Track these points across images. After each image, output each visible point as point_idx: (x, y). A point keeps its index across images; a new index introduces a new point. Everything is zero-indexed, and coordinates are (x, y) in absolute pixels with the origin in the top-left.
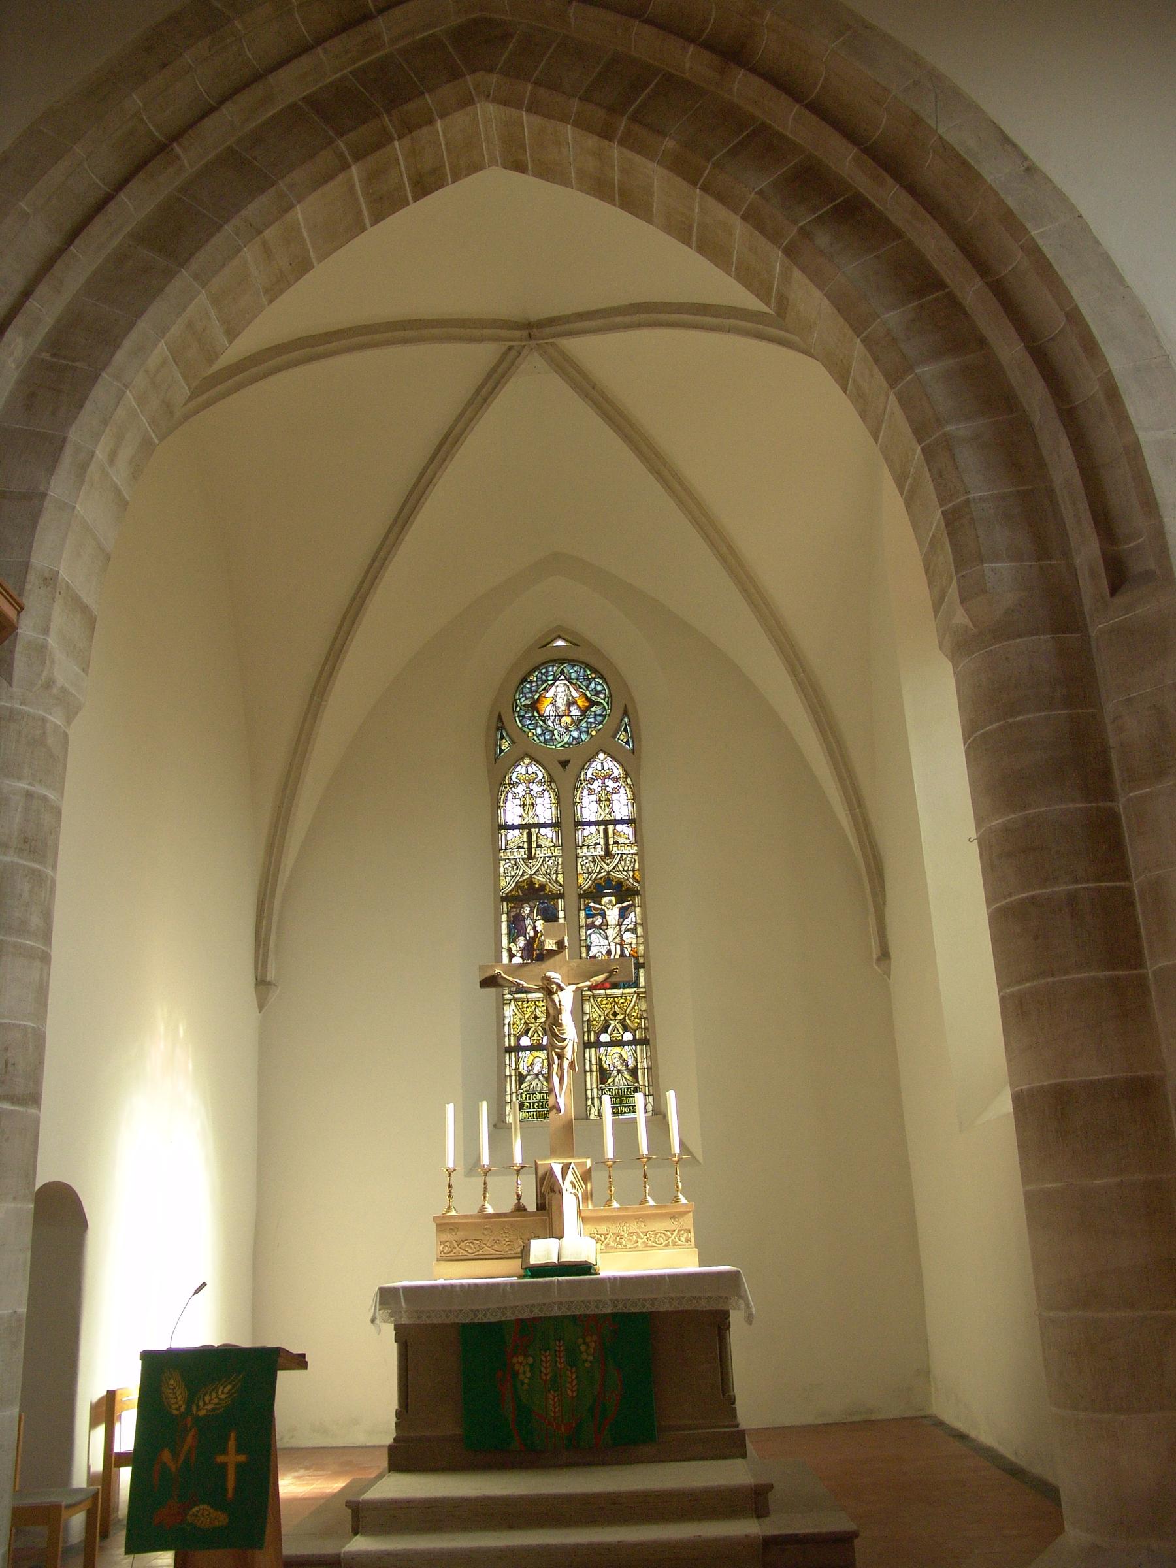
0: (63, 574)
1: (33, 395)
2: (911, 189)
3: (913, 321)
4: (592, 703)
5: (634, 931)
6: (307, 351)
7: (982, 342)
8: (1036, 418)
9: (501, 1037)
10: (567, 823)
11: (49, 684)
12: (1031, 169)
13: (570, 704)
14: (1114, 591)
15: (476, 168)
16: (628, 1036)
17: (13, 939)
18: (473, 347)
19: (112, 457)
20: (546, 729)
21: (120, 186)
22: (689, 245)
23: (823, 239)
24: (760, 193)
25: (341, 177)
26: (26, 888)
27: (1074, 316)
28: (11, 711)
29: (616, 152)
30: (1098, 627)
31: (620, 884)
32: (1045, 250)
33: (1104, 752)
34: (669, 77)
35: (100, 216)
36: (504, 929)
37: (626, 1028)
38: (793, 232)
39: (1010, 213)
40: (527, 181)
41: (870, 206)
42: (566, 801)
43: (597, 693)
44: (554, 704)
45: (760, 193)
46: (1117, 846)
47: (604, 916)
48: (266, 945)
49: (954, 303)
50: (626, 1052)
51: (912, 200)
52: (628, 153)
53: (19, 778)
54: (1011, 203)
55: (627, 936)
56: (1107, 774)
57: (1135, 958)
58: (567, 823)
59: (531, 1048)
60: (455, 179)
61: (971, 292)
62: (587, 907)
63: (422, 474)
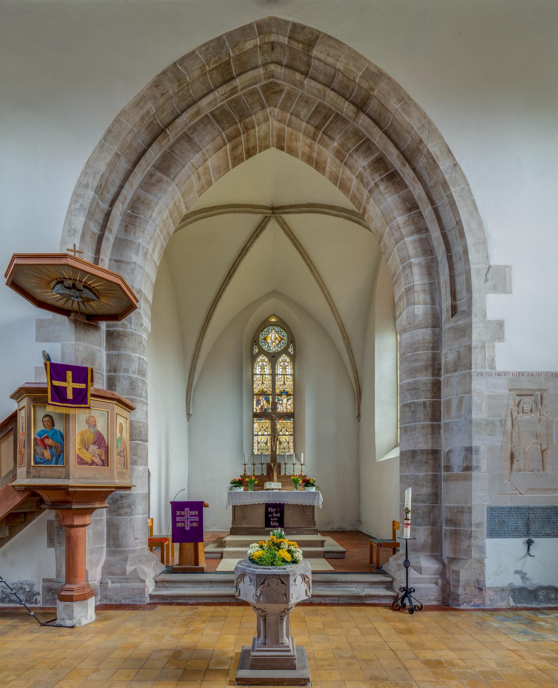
0: (143, 290)
1: (127, 226)
2: (414, 170)
3: (406, 221)
4: (282, 339)
5: (290, 405)
6: (204, 214)
7: (427, 230)
8: (439, 259)
9: (253, 432)
10: (273, 375)
11: (142, 325)
12: (456, 165)
13: (276, 339)
14: (452, 316)
16: (287, 433)
17: (138, 398)
18: (255, 215)
19: (154, 250)
20: (268, 346)
21: (149, 146)
22: (336, 186)
23: (382, 187)
24: (364, 167)
25: (224, 148)
26: (141, 384)
27: (459, 223)
28: (132, 333)
29: (316, 146)
30: (446, 326)
31: (287, 392)
32: (455, 197)
33: (440, 364)
34: (337, 115)
35: (143, 157)
37: (287, 431)
38: (372, 184)
39: (445, 182)
40: (284, 154)
41: (399, 175)
42: (273, 368)
43: (284, 336)
44: (271, 339)
45: (364, 167)
46: (439, 390)
47: (282, 400)
48: (189, 404)
49: (420, 215)
50: (286, 437)
51: (414, 175)
52: (320, 146)
53: (136, 353)
54: (447, 177)
55: (288, 406)
56: (440, 369)
57: (439, 419)
58: (273, 375)
59: (262, 435)
60: (260, 152)
61: (427, 211)
62: (278, 398)
63: (236, 261)
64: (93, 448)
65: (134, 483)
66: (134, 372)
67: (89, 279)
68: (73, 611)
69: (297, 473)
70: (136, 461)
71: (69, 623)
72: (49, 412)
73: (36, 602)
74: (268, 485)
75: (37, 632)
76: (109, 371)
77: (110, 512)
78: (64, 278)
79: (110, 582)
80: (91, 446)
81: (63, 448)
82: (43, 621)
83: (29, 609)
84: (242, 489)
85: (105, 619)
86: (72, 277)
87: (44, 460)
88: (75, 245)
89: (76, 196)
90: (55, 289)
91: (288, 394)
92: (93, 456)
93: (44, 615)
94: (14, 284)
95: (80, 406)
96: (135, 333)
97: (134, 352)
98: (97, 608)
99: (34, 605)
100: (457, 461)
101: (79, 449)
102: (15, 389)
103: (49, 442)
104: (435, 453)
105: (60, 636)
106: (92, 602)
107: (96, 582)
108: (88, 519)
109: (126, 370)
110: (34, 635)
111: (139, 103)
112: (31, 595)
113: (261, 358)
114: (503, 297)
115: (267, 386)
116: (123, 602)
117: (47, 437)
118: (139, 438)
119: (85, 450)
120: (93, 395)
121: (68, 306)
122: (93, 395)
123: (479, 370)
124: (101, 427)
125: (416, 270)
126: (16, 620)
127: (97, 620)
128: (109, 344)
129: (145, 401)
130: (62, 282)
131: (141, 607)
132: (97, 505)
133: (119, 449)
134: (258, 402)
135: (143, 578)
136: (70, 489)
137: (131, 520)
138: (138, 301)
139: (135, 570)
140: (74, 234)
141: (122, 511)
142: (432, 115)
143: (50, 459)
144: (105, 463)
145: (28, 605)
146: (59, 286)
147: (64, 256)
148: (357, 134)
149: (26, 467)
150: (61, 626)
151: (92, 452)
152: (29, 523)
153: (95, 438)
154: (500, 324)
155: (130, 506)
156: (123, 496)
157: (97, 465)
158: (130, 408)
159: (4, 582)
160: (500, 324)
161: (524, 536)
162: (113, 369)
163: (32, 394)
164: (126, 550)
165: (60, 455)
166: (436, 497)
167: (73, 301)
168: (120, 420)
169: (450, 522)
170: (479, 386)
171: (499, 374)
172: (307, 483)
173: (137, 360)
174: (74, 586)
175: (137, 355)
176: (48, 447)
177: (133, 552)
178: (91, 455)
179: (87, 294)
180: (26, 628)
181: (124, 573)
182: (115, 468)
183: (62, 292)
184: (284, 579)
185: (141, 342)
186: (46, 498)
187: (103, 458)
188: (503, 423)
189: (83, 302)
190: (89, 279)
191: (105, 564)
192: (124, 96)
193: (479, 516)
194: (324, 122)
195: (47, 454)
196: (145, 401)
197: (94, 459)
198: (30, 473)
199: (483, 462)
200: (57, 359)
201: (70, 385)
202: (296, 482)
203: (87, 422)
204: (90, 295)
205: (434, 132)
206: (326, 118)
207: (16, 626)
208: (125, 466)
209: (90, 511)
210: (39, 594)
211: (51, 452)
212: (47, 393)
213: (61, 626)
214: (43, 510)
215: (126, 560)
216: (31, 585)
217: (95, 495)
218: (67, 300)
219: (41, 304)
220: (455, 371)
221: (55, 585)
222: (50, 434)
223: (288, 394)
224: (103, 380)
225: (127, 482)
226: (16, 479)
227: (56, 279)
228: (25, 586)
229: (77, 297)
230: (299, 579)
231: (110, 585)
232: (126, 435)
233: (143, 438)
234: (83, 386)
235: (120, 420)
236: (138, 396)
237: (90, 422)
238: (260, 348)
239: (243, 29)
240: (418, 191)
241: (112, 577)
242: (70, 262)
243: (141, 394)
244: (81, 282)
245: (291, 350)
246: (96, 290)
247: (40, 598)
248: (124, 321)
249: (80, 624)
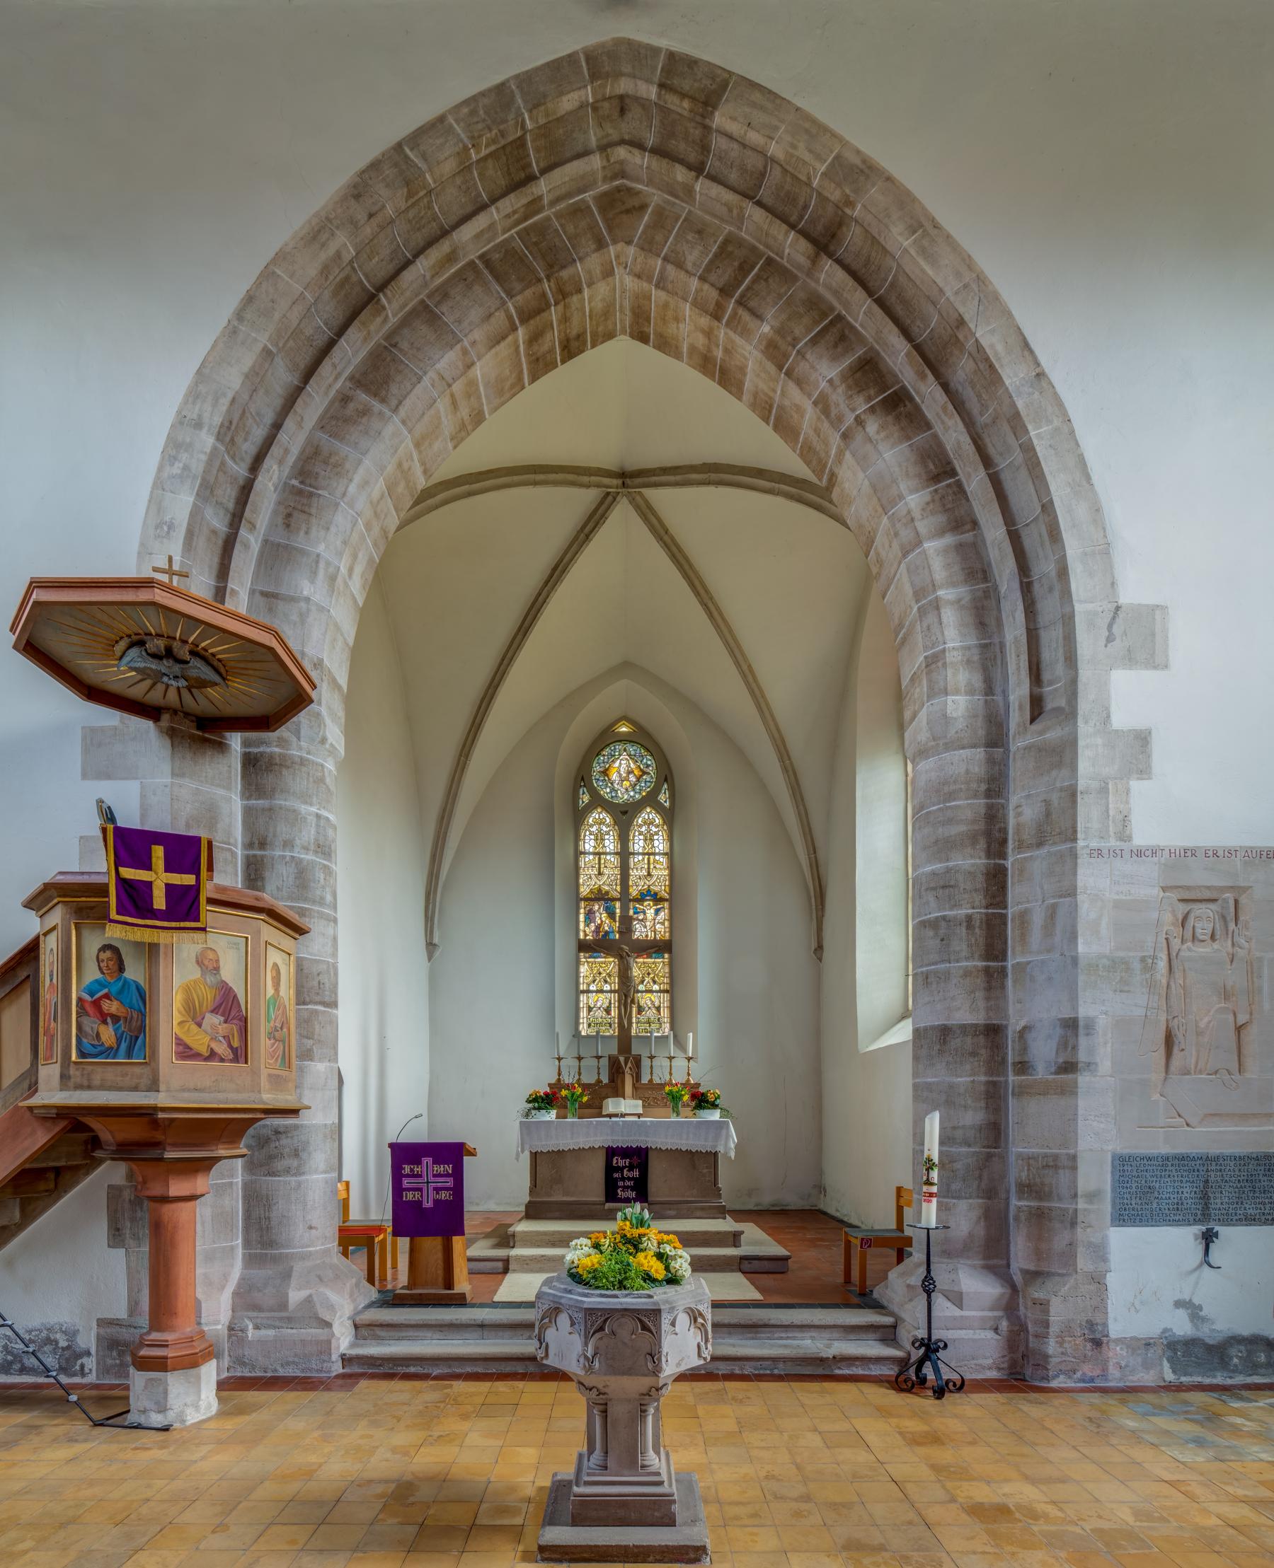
0: (326, 662)
1: (289, 515)
2: (945, 387)
3: (928, 504)
4: (644, 773)
5: (663, 924)
6: (466, 488)
7: (975, 524)
8: (1003, 589)
9: (577, 984)
10: (624, 854)
11: (324, 741)
12: (1040, 375)
13: (630, 772)
14: (1032, 721)
15: (610, 336)
16: (656, 987)
17: (316, 908)
18: (583, 491)
19: (351, 570)
20: (613, 790)
21: (341, 332)
22: (768, 423)
23: (872, 427)
26: (322, 876)
27: (1048, 508)
28: (301, 758)
29: (722, 333)
30: (1017, 743)
31: (656, 894)
32: (1038, 449)
34: (770, 261)
35: (327, 359)
36: (582, 917)
37: (655, 982)
38: (850, 419)
39: (1017, 415)
40: (648, 352)
41: (911, 399)
42: (624, 839)
43: (648, 766)
44: (619, 772)
45: (830, 381)
46: (1003, 888)
47: (644, 913)
48: (432, 920)
49: (960, 489)
50: (654, 997)
51: (945, 398)
52: (731, 334)
53: (311, 805)
54: (1020, 404)
55: (658, 926)
56: (1004, 842)
57: (1002, 956)
58: (624, 854)
59: (597, 992)
60: (593, 347)
61: (975, 481)
63: (539, 594)
64: (213, 1020)
65: (306, 1102)
66: (306, 849)
67: (202, 637)
68: (166, 1392)
69: (679, 1078)
70: (310, 1050)
71: (156, 1419)
72: (112, 938)
73: (82, 1372)
74: (611, 1105)
75: (86, 1441)
76: (249, 845)
78: (146, 634)
79: (251, 1327)
80: (208, 1015)
81: (143, 1021)
82: (98, 1415)
83: (67, 1389)
84: (552, 1115)
85: (240, 1411)
87: (99, 1049)
88: (170, 559)
89: (174, 447)
90: (126, 659)
91: (657, 899)
92: (213, 1039)
93: (102, 1401)
94: (32, 648)
95: (182, 924)
96: (308, 760)
97: (306, 803)
98: (222, 1386)
99: (77, 1380)
100: (1043, 1051)
101: (180, 1024)
102: (34, 886)
103: (112, 1007)
104: (993, 1032)
105: (136, 1449)
106: (210, 1373)
107: (219, 1327)
108: (201, 1183)
109: (288, 844)
110: (79, 1448)
111: (316, 234)
112: (71, 1357)
113: (596, 815)
114: (1149, 676)
115: (609, 880)
116: (281, 1372)
117: (107, 996)
118: (318, 998)
119: (194, 1027)
120: (211, 901)
121: (155, 697)
122: (211, 901)
123: (1094, 844)
124: (231, 972)
125: (949, 616)
126: (36, 1413)
127: (221, 1414)
128: (250, 784)
129: (332, 913)
130: (141, 643)
131: (322, 1383)
132: (222, 1152)
133: (272, 1024)
134: (590, 915)
135: (327, 1318)
136: (161, 1115)
137: (299, 1184)
138: (314, 687)
139: (309, 1300)
140: (168, 533)
141: (280, 1165)
142: (987, 263)
143: (115, 1046)
144: (240, 1054)
145: (64, 1379)
146: (134, 652)
147: (147, 584)
148: (815, 305)
149: (58, 1065)
150: (139, 1427)
151: (209, 1030)
152: (66, 1192)
153: (218, 998)
154: (1142, 739)
155: (296, 1154)
156: (281, 1130)
157: (222, 1060)
158: (298, 930)
159: (10, 1326)
160: (1142, 739)
161: (1196, 1222)
162: (258, 841)
163: (73, 898)
164: (287, 1254)
165: (137, 1038)
166: (995, 1132)
167: (168, 686)
168: (274, 957)
169: (1027, 1189)
170: (1093, 879)
171: (1140, 853)
172: (701, 1101)
173: (312, 820)
174: (169, 1336)
175: (314, 809)
176: (109, 1020)
177: (304, 1257)
178: (208, 1038)
179: (199, 669)
180: (60, 1430)
181: (283, 1306)
182: (262, 1066)
183: (142, 665)
184: (648, 1321)
185: (321, 780)
186: (105, 1136)
187: (236, 1044)
188: (1148, 965)
189: (189, 689)
190: (202, 637)
191: (239, 1285)
192: (282, 218)
193: (1094, 1176)
194: (741, 277)
195: (108, 1034)
196: (332, 913)
197: (213, 1045)
198: (69, 1077)
199: (1103, 1053)
200: (129, 818)
201: (159, 878)
202: (675, 1098)
203: (198, 962)
204: (206, 673)
205: (991, 300)
206: (744, 269)
207: (36, 1427)
208: (286, 1061)
209: (206, 1165)
210: (88, 1353)
211: (116, 1030)
212: (108, 896)
213: (139, 1427)
214: (98, 1162)
215: (287, 1276)
216: (72, 1334)
217: (218, 1129)
218: (154, 684)
219: (94, 693)
220: (1040, 844)
221: (125, 1334)
222: (114, 990)
223: (657, 899)
224: (236, 866)
225: (289, 1097)
226: (36, 1091)
227: (129, 636)
228: (58, 1336)
229: (176, 677)
230: (683, 1320)
231: (251, 1333)
232: (287, 992)
233: (327, 999)
234: (189, 879)
235: (274, 957)
236: (314, 902)
237: (206, 962)
238: (594, 793)
239: (555, 66)
240: (953, 436)
241: (255, 1314)
242: (160, 596)
243: (322, 898)
244: (185, 642)
245: (663, 798)
246: (219, 660)
247: (90, 1363)
248: (283, 732)
249: (183, 1421)
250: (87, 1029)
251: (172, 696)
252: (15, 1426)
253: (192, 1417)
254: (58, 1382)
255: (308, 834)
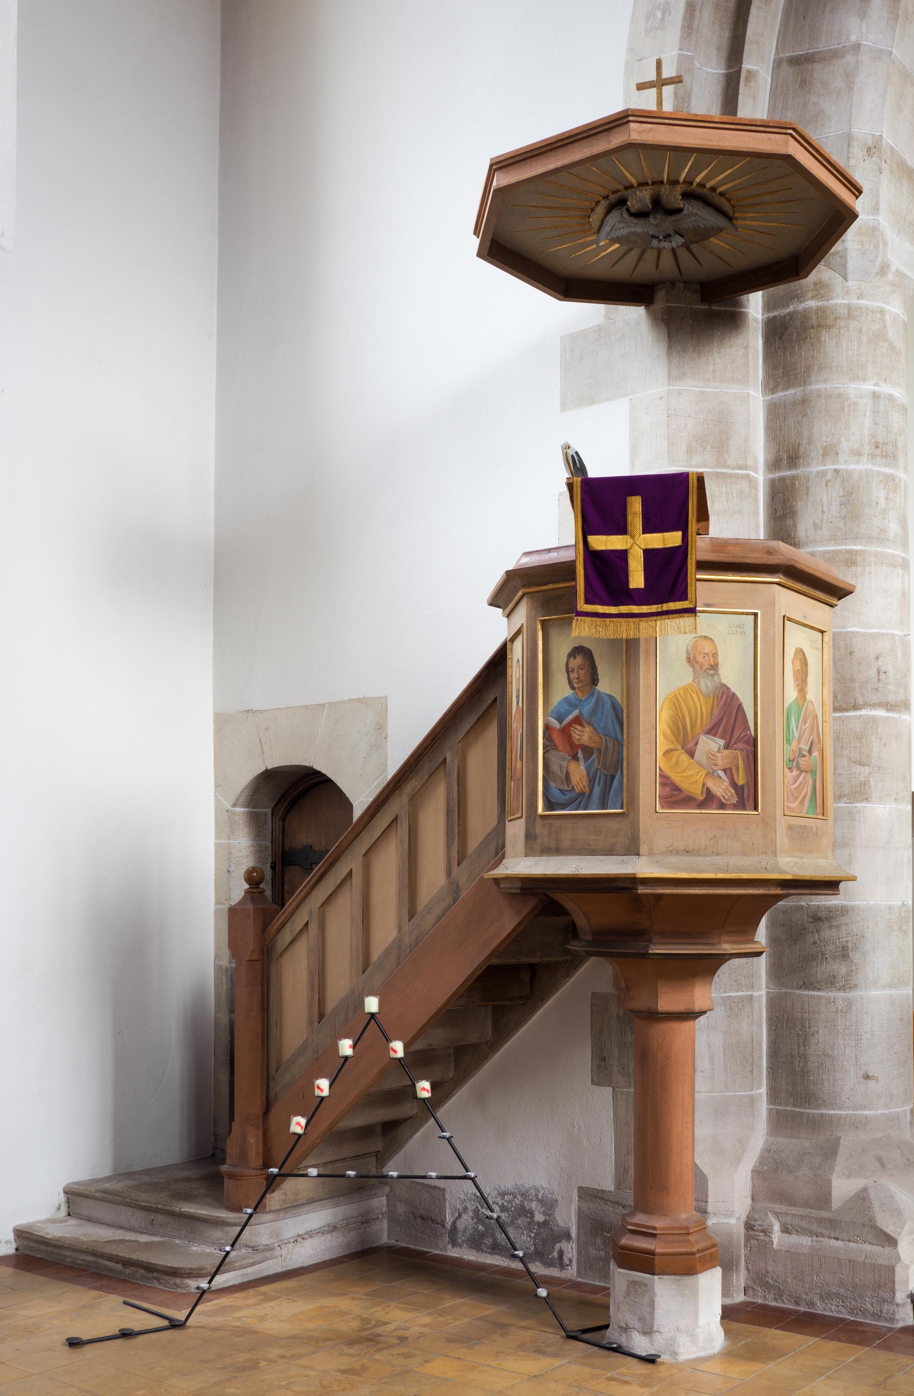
0: (888, 139)
11: (884, 269)
26: (882, 494)
28: (849, 308)
64: (710, 745)
65: (856, 873)
66: (857, 454)
67: (695, 170)
68: (652, 1305)
70: (865, 784)
71: (640, 1344)
72: (580, 638)
73: (561, 1263)
75: (555, 1355)
76: (774, 464)
77: (781, 972)
78: (626, 188)
79: (777, 1227)
80: (703, 739)
81: (620, 753)
82: (574, 1324)
83: (538, 1282)
85: (755, 1354)
86: (649, 177)
87: (570, 795)
88: (659, 63)
90: (606, 229)
92: (710, 774)
93: (584, 1305)
94: (502, 248)
95: (666, 607)
96: (859, 308)
97: (856, 378)
98: (729, 1314)
99: (554, 1272)
101: (667, 753)
102: (495, 579)
103: (583, 735)
105: (611, 1379)
106: (710, 1283)
107: (733, 1221)
108: (701, 995)
109: (830, 452)
110: (545, 1363)
112: (549, 1237)
116: (819, 1309)
117: (577, 720)
118: (876, 698)
119: (685, 757)
120: (704, 566)
121: (646, 271)
122: (704, 566)
124: (734, 674)
126: (503, 1308)
127: (728, 1355)
128: (775, 368)
129: (899, 553)
130: (621, 202)
131: (879, 1336)
132: (727, 947)
133: (794, 746)
135: (890, 1230)
136: (642, 890)
137: (849, 1003)
138: (857, 191)
139: (862, 1197)
140: (663, 18)
141: (821, 971)
143: (587, 790)
144: (747, 796)
145: (537, 1268)
146: (614, 217)
147: (620, 121)
149: (523, 821)
150: (619, 1350)
151: (705, 761)
152: (543, 1000)
153: (716, 711)
155: (844, 954)
156: (822, 914)
157: (722, 806)
158: (833, 592)
159: (473, 1179)
162: (787, 454)
163: (533, 587)
164: (831, 1117)
165: (613, 778)
167: (659, 251)
168: (797, 638)
173: (866, 404)
174: (659, 1223)
175: (869, 387)
176: (580, 755)
177: (858, 1124)
178: (703, 773)
179: (697, 215)
180: (527, 1335)
181: (823, 1199)
182: (779, 813)
183: (624, 232)
185: (881, 335)
186: (581, 921)
187: (741, 780)
189: (687, 246)
190: (695, 170)
191: (762, 1160)
195: (579, 773)
196: (899, 553)
197: (711, 784)
198: (535, 836)
200: (598, 468)
201: (636, 543)
203: (689, 660)
204: (708, 218)
207: (503, 1326)
208: (818, 803)
209: (708, 966)
210: (568, 1237)
211: (588, 768)
212: (574, 579)
213: (619, 1350)
214: (575, 962)
215: (830, 1152)
216: (549, 1205)
217: (717, 914)
218: (643, 253)
219: (568, 286)
221: (613, 1215)
222: (586, 709)
224: (756, 500)
225: (822, 862)
226: (503, 857)
227: (606, 197)
228: (534, 1205)
229: (667, 237)
231: (777, 1236)
232: (818, 692)
233: (891, 698)
234: (673, 539)
235: (797, 638)
236: (870, 539)
237: (700, 659)
241: (784, 1208)
242: (637, 133)
243: (882, 531)
244: (674, 182)
246: (722, 194)
247: (570, 1250)
248: (821, 272)
249: (675, 1354)
250: (555, 768)
251: (667, 260)
252: (479, 1319)
253: (687, 1351)
254: (528, 1270)
255: (858, 430)
